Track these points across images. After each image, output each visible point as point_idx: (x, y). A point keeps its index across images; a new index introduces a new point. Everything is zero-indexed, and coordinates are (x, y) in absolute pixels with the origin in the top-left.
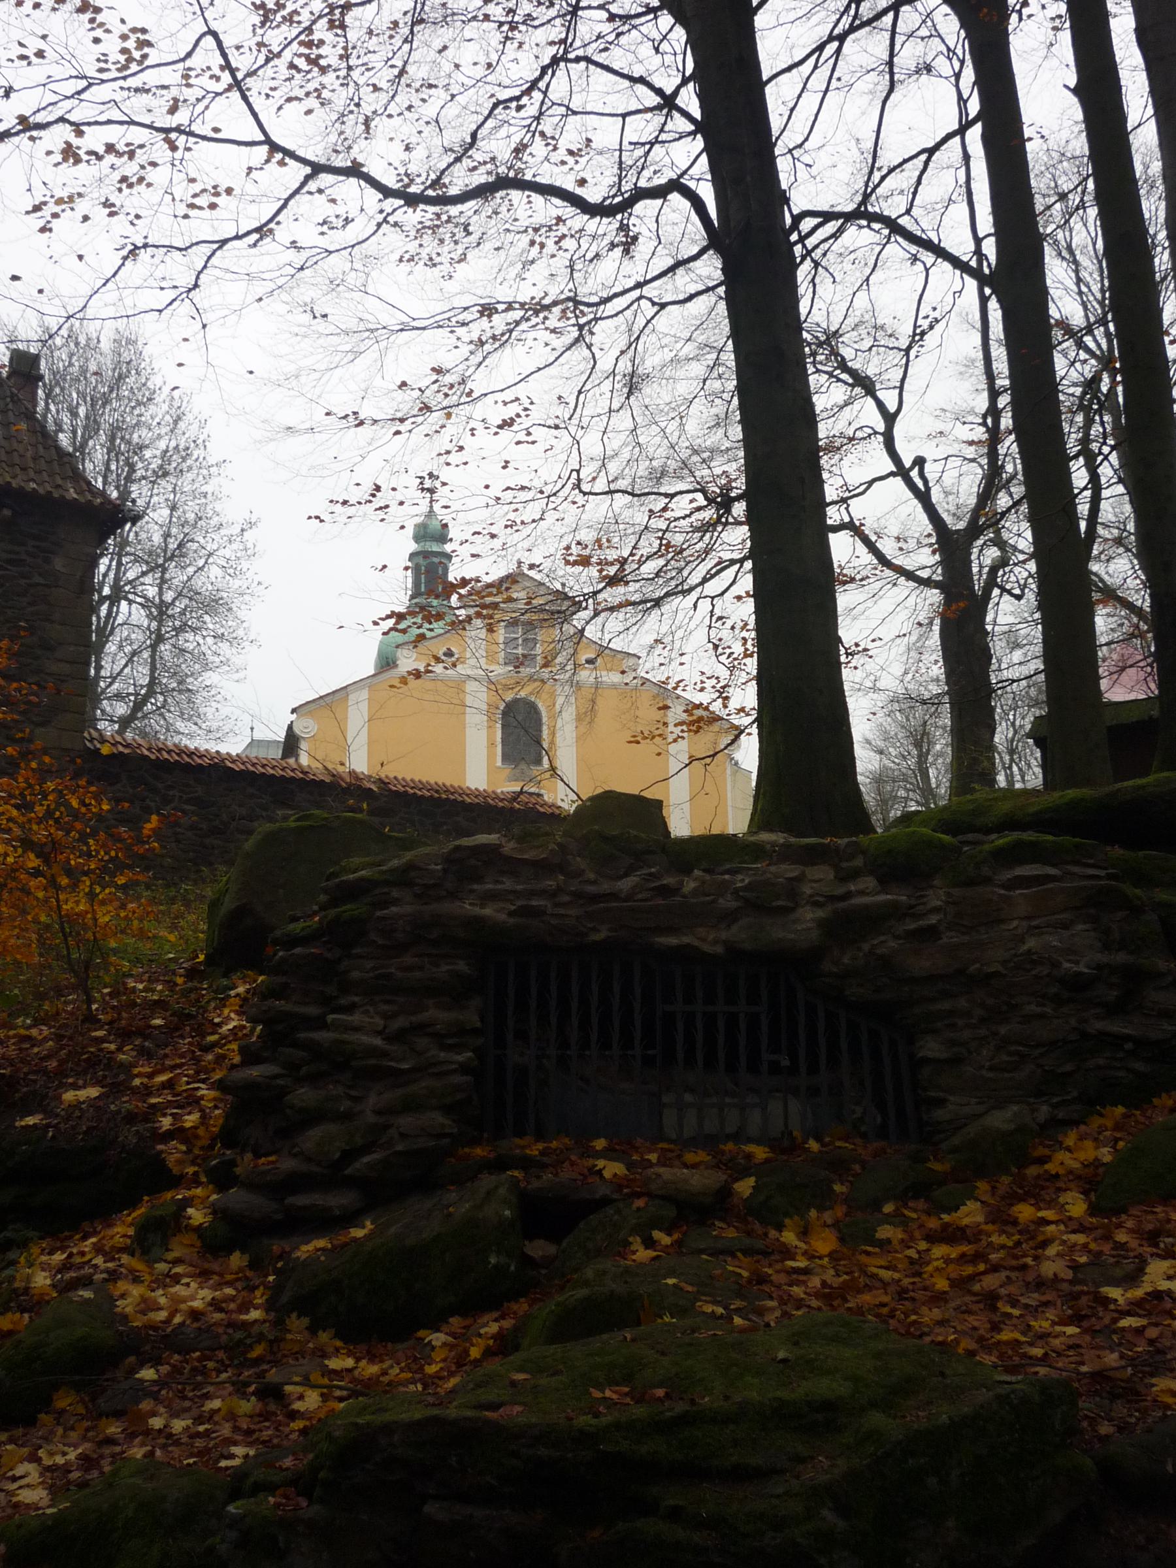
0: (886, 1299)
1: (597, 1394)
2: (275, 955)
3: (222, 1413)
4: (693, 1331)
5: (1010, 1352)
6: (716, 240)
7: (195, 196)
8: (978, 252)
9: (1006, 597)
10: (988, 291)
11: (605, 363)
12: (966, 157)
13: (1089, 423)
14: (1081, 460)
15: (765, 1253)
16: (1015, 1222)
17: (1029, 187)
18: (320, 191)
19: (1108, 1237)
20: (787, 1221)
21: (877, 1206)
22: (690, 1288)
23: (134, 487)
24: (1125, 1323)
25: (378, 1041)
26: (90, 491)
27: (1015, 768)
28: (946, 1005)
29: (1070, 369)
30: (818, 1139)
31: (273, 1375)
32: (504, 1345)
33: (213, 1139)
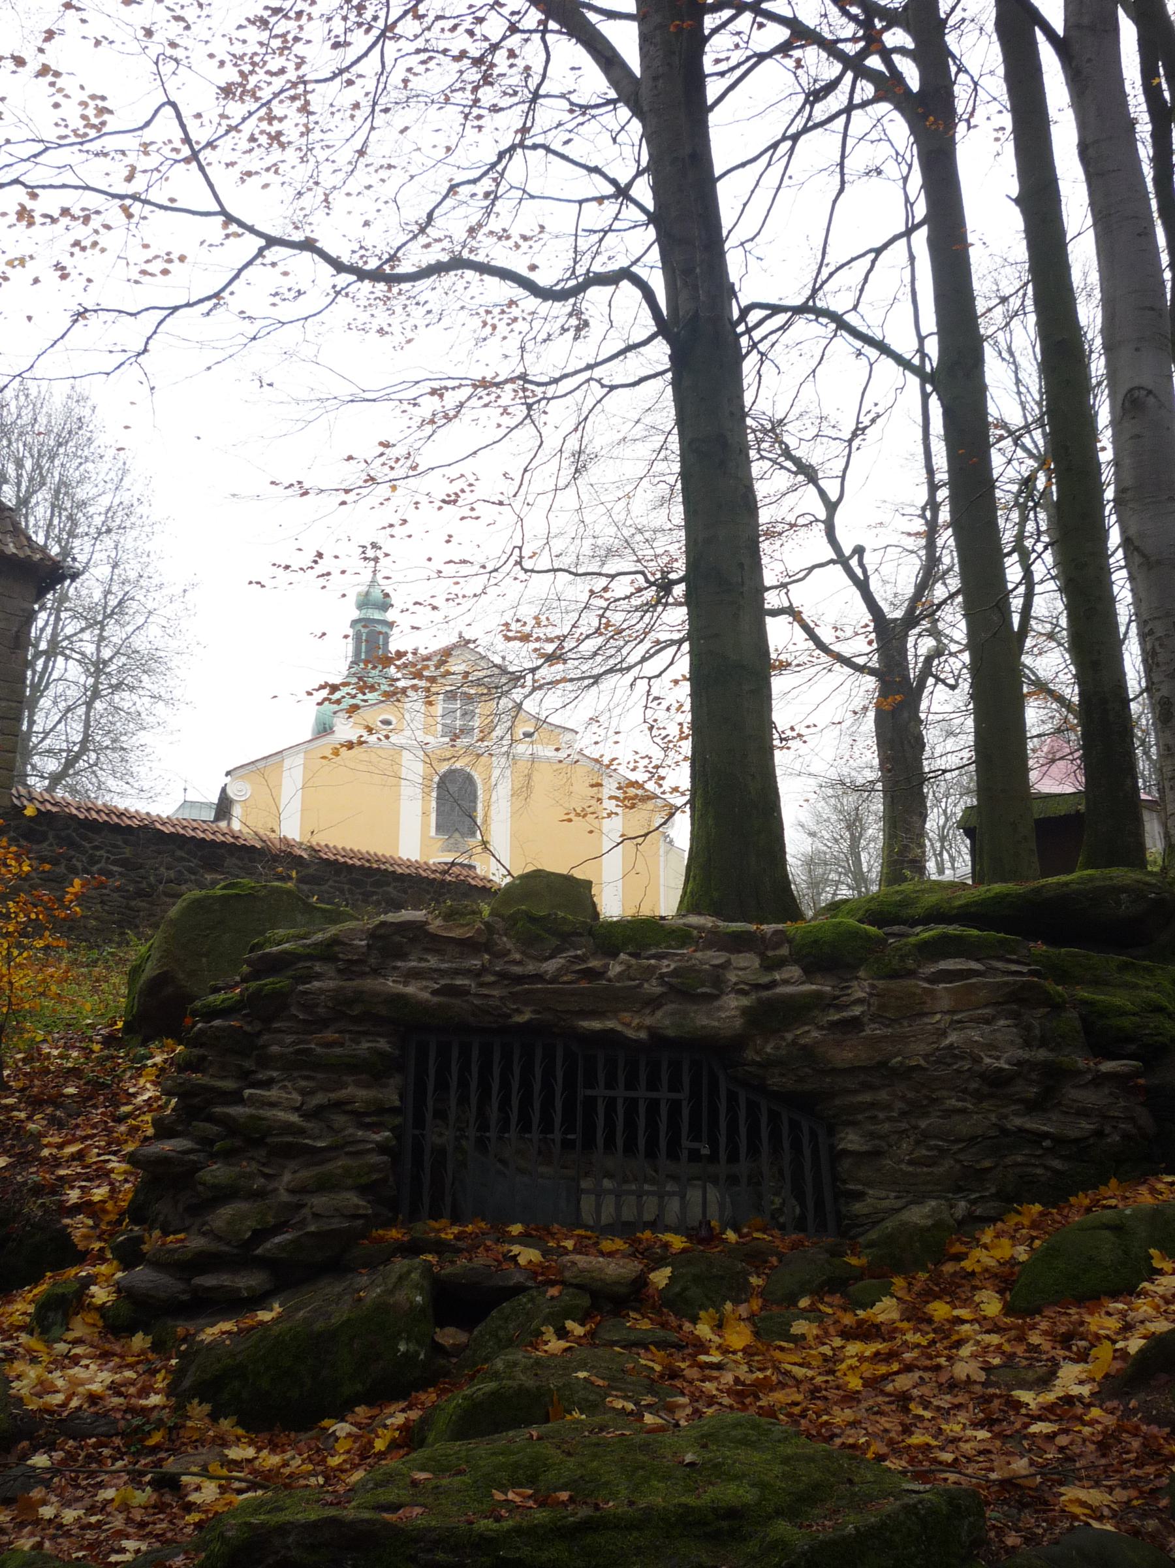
0: (799, 1398)
1: (499, 1496)
2: (194, 1025)
3: (116, 1504)
4: (601, 1430)
5: (920, 1456)
6: (664, 328)
7: (148, 261)
8: (921, 350)
9: (940, 686)
10: (929, 388)
11: (552, 441)
12: (912, 258)
13: (1024, 519)
14: (1015, 557)
15: (679, 1347)
16: (930, 1320)
17: (971, 290)
18: (274, 264)
19: (1021, 1339)
20: (702, 1314)
21: (793, 1300)
22: (600, 1382)
23: (76, 543)
24: (1035, 1428)
25: (294, 1118)
26: (30, 546)
27: (946, 856)
28: (867, 1097)
29: (1009, 466)
30: (737, 1230)
31: (171, 1465)
32: (410, 1438)
33: (122, 1214)
